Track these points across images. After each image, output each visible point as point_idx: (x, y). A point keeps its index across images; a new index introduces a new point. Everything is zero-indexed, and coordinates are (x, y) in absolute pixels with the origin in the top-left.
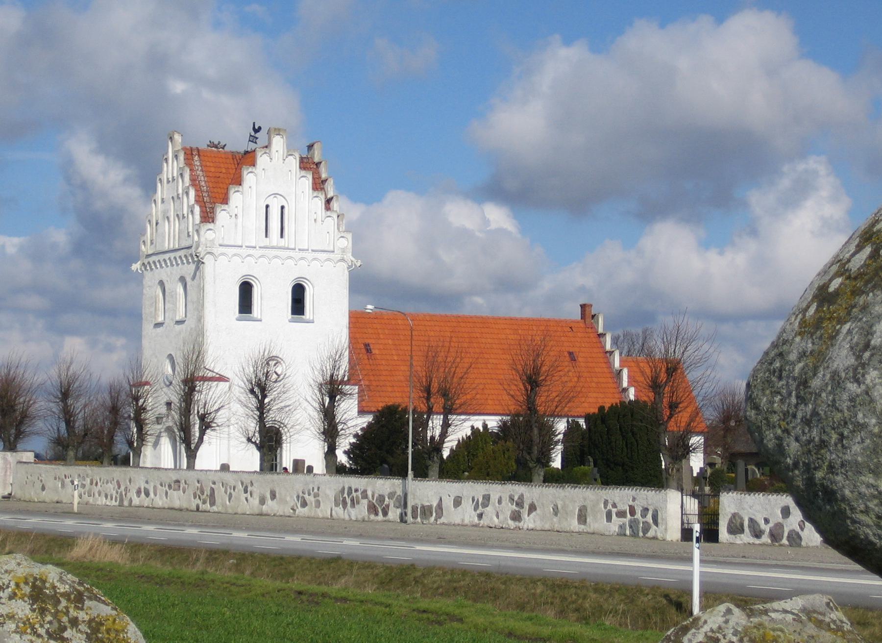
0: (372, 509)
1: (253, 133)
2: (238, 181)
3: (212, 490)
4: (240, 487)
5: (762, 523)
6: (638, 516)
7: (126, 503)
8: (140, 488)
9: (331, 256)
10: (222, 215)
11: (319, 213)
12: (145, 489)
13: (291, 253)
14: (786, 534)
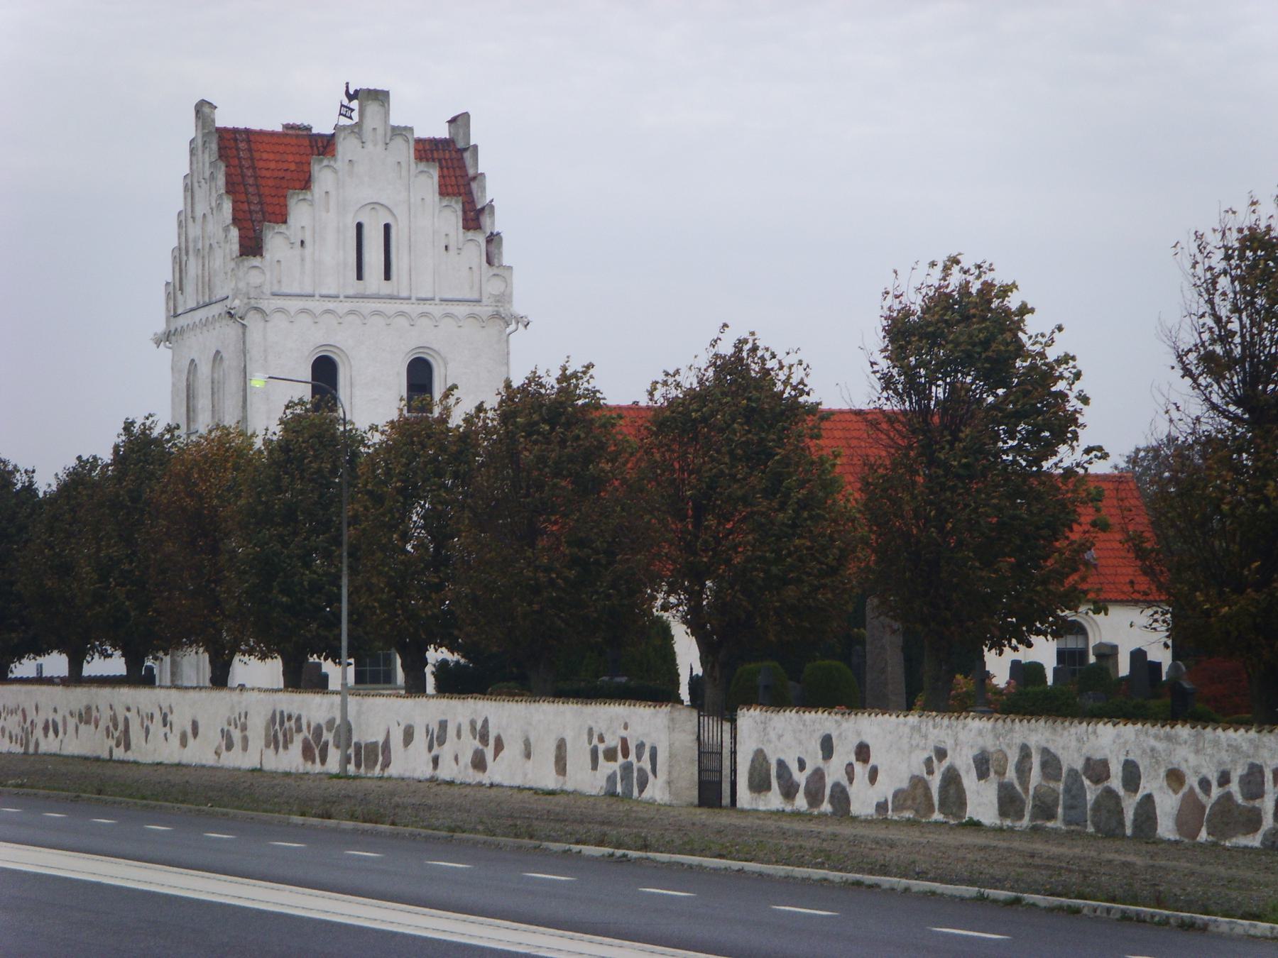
0: (307, 753)
1: (346, 102)
2: (305, 183)
3: (126, 720)
4: (158, 718)
5: (794, 767)
6: (632, 757)
7: (31, 750)
8: (47, 722)
9: (477, 309)
10: (276, 242)
11: (452, 234)
12: (54, 721)
13: (405, 307)
14: (828, 791)
